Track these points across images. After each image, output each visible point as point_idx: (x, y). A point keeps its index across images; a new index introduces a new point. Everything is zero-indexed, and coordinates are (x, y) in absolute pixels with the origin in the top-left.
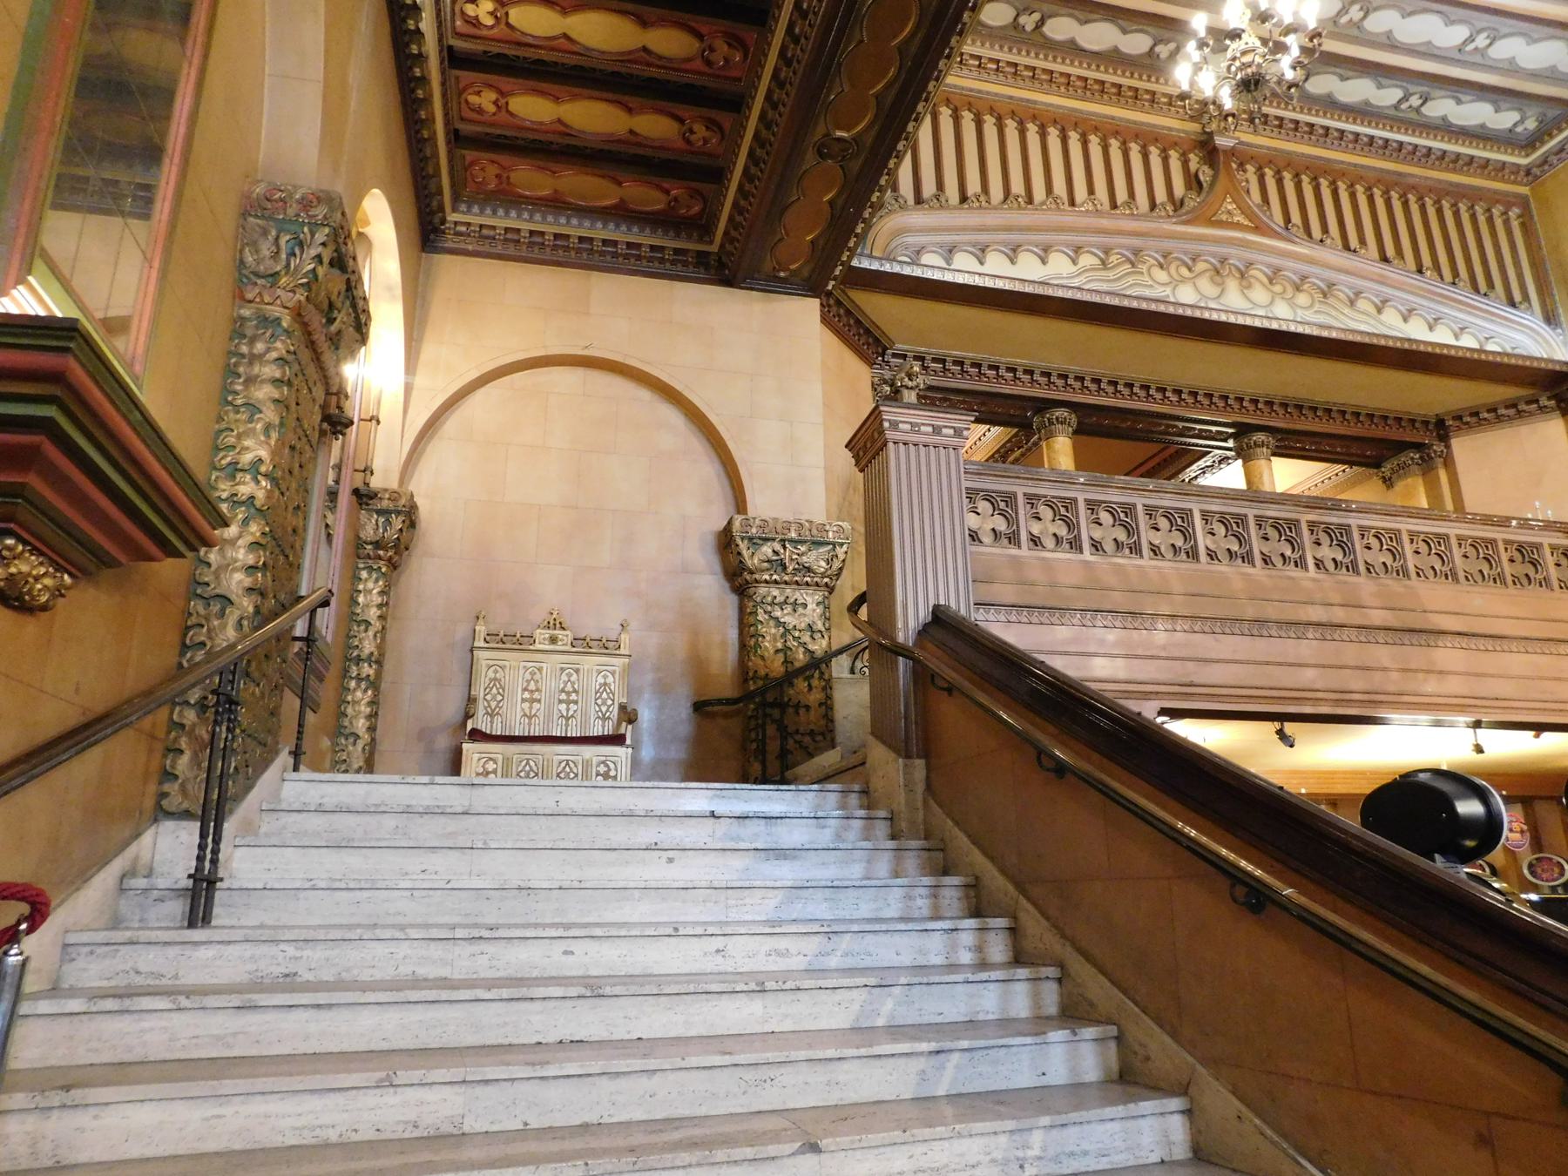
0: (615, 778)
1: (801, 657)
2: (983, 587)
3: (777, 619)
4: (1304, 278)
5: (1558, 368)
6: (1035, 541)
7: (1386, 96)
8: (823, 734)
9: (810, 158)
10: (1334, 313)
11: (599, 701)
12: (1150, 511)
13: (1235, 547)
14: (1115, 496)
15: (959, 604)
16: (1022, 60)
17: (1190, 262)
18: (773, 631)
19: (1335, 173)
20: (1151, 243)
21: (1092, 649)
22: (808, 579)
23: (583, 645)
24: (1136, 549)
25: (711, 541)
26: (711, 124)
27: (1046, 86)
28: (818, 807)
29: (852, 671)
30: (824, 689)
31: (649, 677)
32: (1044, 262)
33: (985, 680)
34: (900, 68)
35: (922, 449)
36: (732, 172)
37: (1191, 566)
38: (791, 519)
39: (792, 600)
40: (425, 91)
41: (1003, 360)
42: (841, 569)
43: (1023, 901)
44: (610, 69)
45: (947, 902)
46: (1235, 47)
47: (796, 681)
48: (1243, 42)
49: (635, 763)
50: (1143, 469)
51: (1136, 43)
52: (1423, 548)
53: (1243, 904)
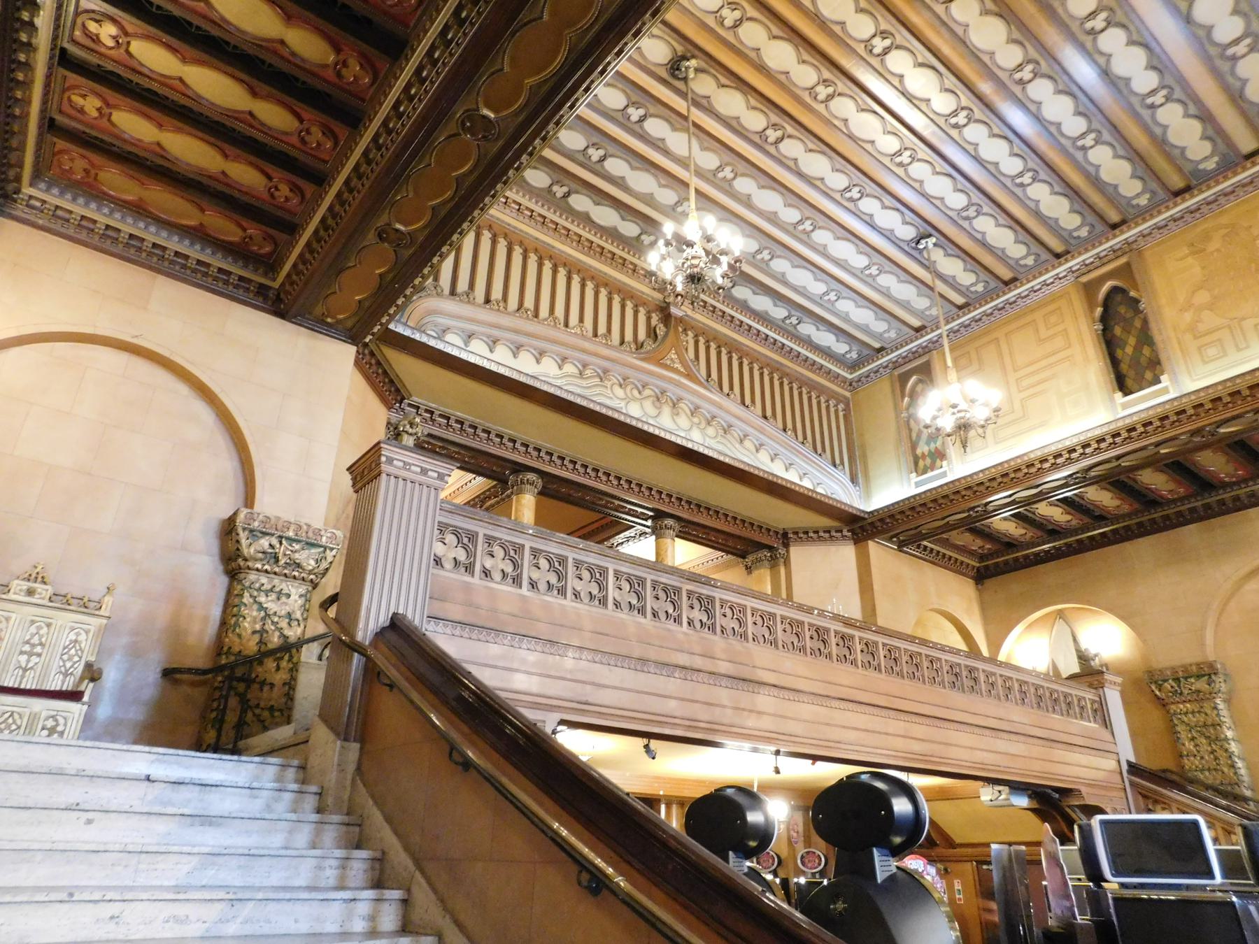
0: (62, 733)
1: (275, 640)
2: (437, 604)
3: (260, 604)
4: (714, 417)
5: (855, 512)
6: (486, 573)
7: (779, 313)
8: (281, 710)
9: (371, 237)
10: (729, 445)
11: (65, 657)
12: (578, 564)
13: (634, 602)
14: (554, 549)
15: (415, 616)
16: (550, 215)
17: (640, 388)
18: (255, 613)
19: (743, 353)
20: (618, 367)
21: (515, 666)
22: (296, 574)
23: (62, 601)
24: (562, 592)
25: (214, 527)
26: (295, 188)
27: (563, 238)
28: (257, 778)
29: (320, 658)
30: (291, 670)
31: (125, 640)
32: (538, 362)
33: (420, 680)
34: (455, 192)
35: (409, 484)
36: (304, 230)
37: (601, 611)
38: (292, 520)
39: (278, 590)
40: (26, 76)
41: (495, 427)
42: (327, 569)
43: (418, 875)
44: (216, 119)
45: (354, 873)
46: (689, 252)
47: (266, 660)
48: (694, 250)
49: (88, 720)
50: (580, 533)
51: (630, 229)
52: (759, 621)
53: (586, 887)
